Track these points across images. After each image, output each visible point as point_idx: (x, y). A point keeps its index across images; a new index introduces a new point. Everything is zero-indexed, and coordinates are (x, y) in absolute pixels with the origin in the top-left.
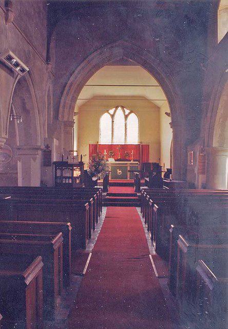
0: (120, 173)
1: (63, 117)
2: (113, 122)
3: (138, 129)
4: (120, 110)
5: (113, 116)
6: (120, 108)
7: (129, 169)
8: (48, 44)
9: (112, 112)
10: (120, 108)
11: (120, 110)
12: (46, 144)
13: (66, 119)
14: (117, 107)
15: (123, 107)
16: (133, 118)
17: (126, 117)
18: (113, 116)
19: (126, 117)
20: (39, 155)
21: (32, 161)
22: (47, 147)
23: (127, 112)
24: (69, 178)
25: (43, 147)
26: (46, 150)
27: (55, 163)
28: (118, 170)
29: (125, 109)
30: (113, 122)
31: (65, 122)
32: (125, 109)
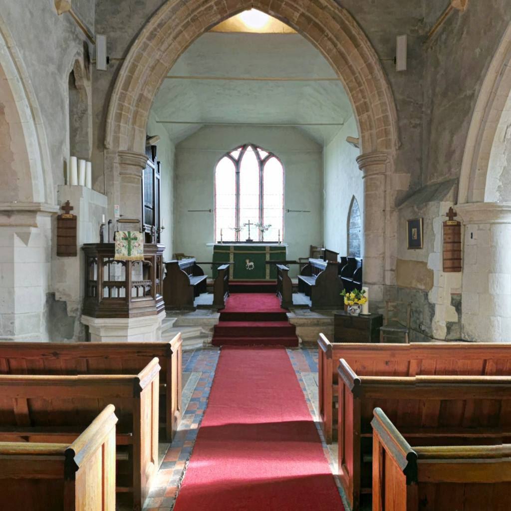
0: (251, 266)
1: (117, 140)
2: (238, 173)
3: (282, 197)
4: (250, 151)
5: (237, 163)
6: (250, 148)
7: (268, 258)
8: (197, 123)
9: (235, 154)
10: (250, 148)
11: (250, 151)
12: (63, 201)
13: (123, 147)
14: (244, 147)
15: (255, 147)
16: (275, 167)
17: (262, 163)
18: (237, 163)
19: (262, 163)
20: (44, 225)
21: (17, 241)
22: (67, 207)
23: (263, 154)
24: (119, 285)
25: (56, 209)
26: (450, 223)
27: (87, 248)
28: (247, 261)
29: (258, 149)
30: (238, 173)
31: (121, 154)
32: (258, 149)
